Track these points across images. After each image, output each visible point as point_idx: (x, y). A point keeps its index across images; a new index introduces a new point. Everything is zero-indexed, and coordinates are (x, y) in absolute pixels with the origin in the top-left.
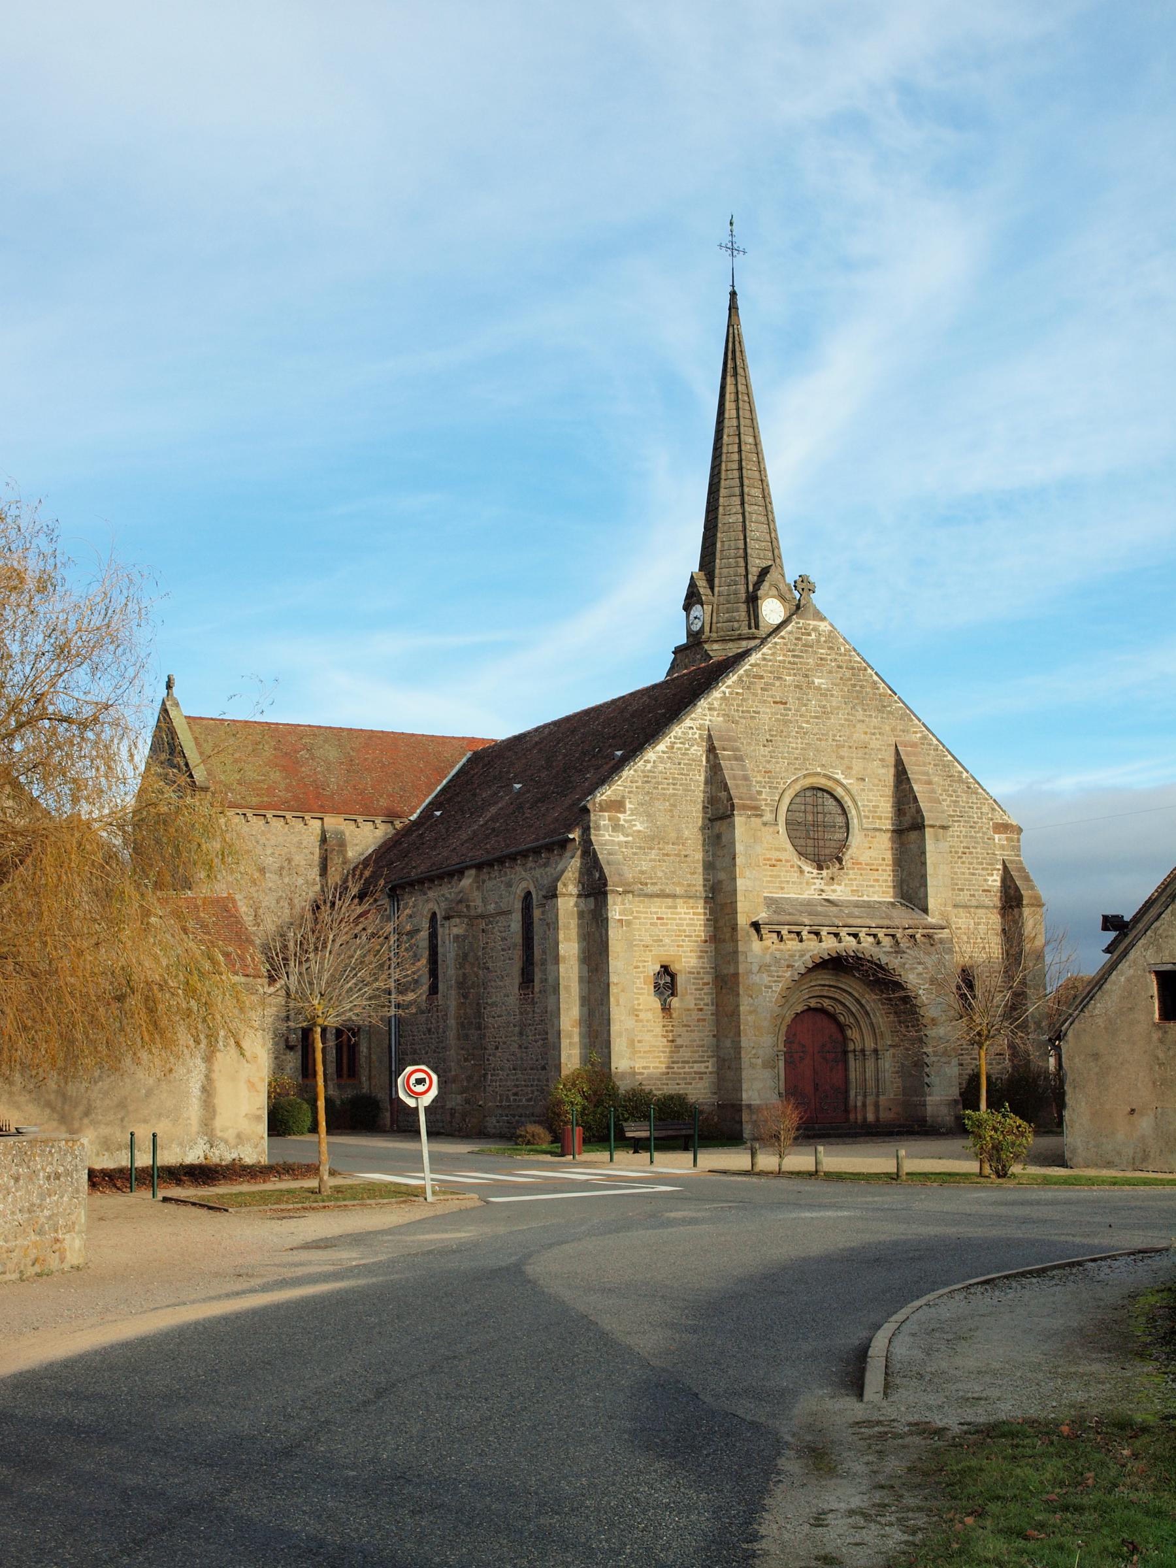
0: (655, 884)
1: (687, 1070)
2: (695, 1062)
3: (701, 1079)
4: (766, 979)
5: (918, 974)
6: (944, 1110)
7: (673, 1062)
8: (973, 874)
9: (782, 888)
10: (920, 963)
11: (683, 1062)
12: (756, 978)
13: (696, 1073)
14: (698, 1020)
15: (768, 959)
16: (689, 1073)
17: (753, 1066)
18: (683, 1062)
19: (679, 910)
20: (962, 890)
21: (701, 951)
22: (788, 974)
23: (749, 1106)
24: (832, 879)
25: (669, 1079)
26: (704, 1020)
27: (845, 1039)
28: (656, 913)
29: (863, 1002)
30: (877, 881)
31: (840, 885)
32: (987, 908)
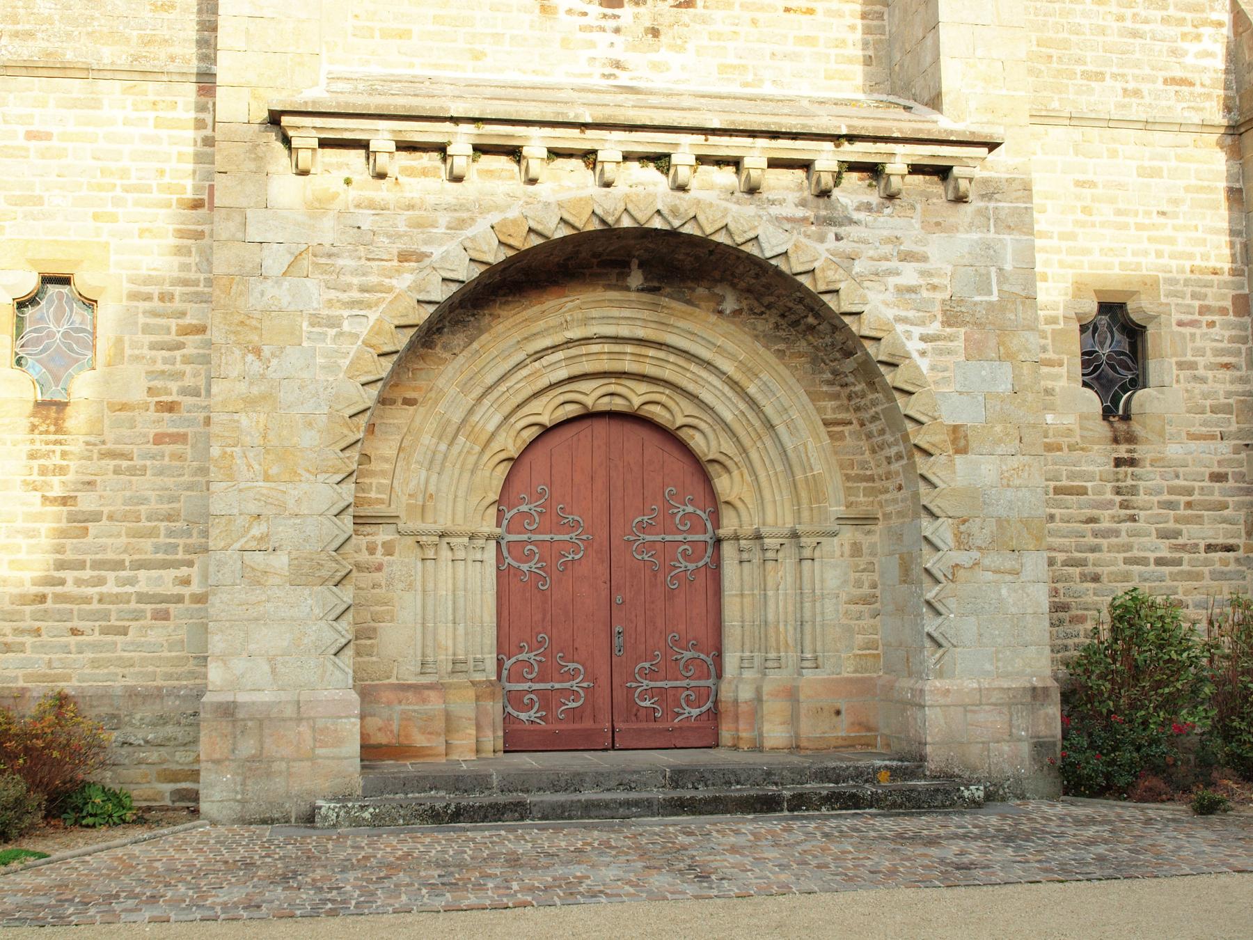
0: (30, 34)
1: (111, 588)
3: (164, 616)
4: (314, 293)
5: (900, 290)
6: (990, 721)
7: (61, 565)
8: (1135, 34)
10: (907, 257)
11: (97, 565)
12: (278, 294)
13: (142, 598)
14: (159, 439)
15: (328, 232)
16: (117, 599)
17: (256, 579)
18: (97, 565)
20: (1100, 76)
21: (182, 234)
22: (404, 281)
23: (228, 711)
24: (655, 32)
25: (45, 616)
26: (180, 438)
27: (714, 504)
29: (752, 390)
30: (810, 40)
31: (681, 49)
32: (1181, 127)
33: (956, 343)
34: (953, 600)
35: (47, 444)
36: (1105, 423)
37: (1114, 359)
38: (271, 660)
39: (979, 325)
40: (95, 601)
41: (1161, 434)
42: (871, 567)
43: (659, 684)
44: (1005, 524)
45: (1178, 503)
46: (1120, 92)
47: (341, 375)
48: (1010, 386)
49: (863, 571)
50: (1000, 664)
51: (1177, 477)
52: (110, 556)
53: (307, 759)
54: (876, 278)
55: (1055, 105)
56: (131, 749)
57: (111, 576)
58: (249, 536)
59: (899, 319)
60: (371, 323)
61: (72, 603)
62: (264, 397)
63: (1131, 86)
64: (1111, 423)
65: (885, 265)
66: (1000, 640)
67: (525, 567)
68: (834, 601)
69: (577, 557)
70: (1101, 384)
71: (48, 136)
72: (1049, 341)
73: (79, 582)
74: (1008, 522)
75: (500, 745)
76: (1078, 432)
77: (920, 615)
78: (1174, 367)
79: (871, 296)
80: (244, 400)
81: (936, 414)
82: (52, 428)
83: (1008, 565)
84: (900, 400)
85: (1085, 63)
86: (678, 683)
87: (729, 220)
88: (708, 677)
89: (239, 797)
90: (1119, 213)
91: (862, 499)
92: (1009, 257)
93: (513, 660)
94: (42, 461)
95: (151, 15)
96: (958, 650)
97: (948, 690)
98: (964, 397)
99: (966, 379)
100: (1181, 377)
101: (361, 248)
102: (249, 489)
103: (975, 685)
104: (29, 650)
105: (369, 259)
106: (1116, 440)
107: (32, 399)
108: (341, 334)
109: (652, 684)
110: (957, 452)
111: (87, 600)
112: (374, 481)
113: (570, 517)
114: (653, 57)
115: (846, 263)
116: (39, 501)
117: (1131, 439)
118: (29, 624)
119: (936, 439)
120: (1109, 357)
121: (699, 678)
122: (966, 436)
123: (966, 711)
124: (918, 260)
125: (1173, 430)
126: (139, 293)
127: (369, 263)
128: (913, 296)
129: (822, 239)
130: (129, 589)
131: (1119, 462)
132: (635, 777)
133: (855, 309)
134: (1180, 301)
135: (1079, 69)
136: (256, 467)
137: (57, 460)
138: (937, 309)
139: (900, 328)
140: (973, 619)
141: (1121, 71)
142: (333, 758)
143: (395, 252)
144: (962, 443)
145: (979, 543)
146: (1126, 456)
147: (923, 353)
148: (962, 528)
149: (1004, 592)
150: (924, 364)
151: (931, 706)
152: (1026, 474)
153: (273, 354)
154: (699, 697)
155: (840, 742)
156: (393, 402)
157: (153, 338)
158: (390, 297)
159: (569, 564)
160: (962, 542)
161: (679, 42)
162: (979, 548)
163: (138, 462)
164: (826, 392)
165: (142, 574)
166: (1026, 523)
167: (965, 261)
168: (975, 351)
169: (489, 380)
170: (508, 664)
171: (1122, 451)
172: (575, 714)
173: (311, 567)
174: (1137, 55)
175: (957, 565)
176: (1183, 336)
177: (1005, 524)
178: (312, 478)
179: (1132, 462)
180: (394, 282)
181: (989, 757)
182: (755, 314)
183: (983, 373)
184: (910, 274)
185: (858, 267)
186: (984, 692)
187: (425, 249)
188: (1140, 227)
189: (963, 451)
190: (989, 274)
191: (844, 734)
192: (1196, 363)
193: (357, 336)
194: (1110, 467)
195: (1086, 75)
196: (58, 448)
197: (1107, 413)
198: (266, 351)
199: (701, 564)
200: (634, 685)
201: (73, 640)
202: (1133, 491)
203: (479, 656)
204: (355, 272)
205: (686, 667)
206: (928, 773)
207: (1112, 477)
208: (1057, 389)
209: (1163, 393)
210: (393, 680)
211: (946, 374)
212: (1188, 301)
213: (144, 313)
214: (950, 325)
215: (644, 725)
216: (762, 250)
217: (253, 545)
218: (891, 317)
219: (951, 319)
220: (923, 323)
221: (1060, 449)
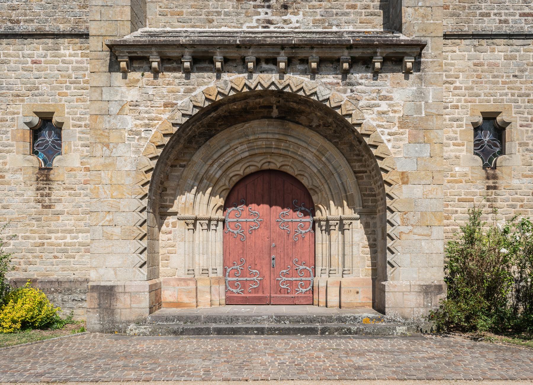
0: (32, 21)
1: (68, 240)
2: (80, 232)
9: (211, 21)
10: (385, 98)
11: (64, 231)
13: (80, 244)
16: (70, 245)
18: (64, 231)
19: (62, 51)
20: (488, 15)
22: (165, 116)
28: (30, 56)
31: (295, 14)
33: (404, 136)
34: (400, 247)
35: (43, 184)
36: (483, 171)
37: (490, 142)
38: (115, 269)
39: (416, 128)
40: (63, 245)
41: (509, 175)
42: (373, 232)
43: (289, 279)
44: (424, 214)
45: (516, 205)
46: (498, 21)
47: (141, 155)
48: (429, 154)
49: (370, 234)
50: (420, 275)
51: (516, 194)
52: (68, 228)
53: (128, 308)
54: (369, 108)
55: (466, 29)
56: (76, 302)
57: (68, 235)
58: (105, 220)
59: (379, 126)
60: (153, 133)
61: (54, 246)
62: (110, 164)
63: (503, 18)
64: (486, 171)
65: (373, 102)
66: (420, 264)
67: (235, 232)
68: (357, 246)
69: (256, 228)
70: (484, 154)
71: (40, 62)
72: (458, 135)
73: (56, 238)
74: (426, 214)
75: (223, 302)
76: (470, 174)
77: (386, 254)
78: (517, 145)
79: (366, 116)
80: (102, 165)
81: (394, 167)
82: (45, 178)
83: (425, 232)
84: (379, 162)
85: (481, 9)
86: (297, 279)
87: (303, 85)
88: (310, 276)
89: (102, 323)
90: (495, 77)
91: (370, 204)
92: (431, 97)
93: (231, 269)
94: (41, 191)
95: (78, 10)
96: (401, 268)
97: (396, 285)
98: (408, 160)
99: (408, 151)
100: (521, 149)
101: (148, 102)
102: (105, 201)
103: (408, 284)
104: (38, 264)
105: (152, 107)
106: (488, 178)
107: (38, 166)
108: (141, 138)
109: (286, 279)
110: (403, 183)
111: (59, 245)
112: (168, 198)
113: (254, 212)
114: (285, 18)
115: (354, 102)
116: (40, 207)
117: (495, 177)
118: (38, 254)
119: (394, 178)
120: (488, 142)
121: (306, 277)
122: (407, 177)
123: (403, 294)
124: (389, 100)
125: (515, 173)
126: (77, 124)
127: (152, 108)
128: (385, 116)
129: (345, 92)
130: (75, 241)
131: (488, 188)
132: (260, 318)
133: (359, 122)
134: (522, 115)
135: (478, 12)
136: (108, 192)
137: (47, 191)
138: (396, 121)
139: (379, 130)
140: (408, 255)
141: (499, 11)
142: (138, 308)
143: (162, 103)
144: (406, 179)
145: (412, 223)
146: (492, 185)
147: (389, 141)
148: (405, 216)
149: (423, 244)
150: (389, 146)
151: (388, 292)
152: (435, 193)
153: (114, 147)
154: (306, 285)
155: (358, 305)
156: (176, 166)
157: (83, 142)
158: (160, 122)
159: (253, 231)
160: (405, 223)
161: (296, 10)
162: (412, 225)
163: (78, 191)
164: (356, 159)
165: (80, 235)
166: (434, 213)
167: (410, 99)
168: (414, 140)
169: (215, 157)
170: (229, 270)
171: (491, 183)
172: (256, 290)
173: (130, 232)
174: (507, 4)
175: (402, 232)
176: (522, 131)
177: (424, 214)
178: (130, 197)
179: (495, 188)
180: (162, 116)
181: (413, 314)
182: (326, 127)
183: (417, 149)
184: (384, 106)
185: (361, 103)
186: (412, 287)
187: (175, 102)
188: (504, 83)
189: (405, 183)
190: (421, 105)
191: (360, 301)
192: (528, 143)
193: (147, 138)
194: (485, 190)
195: (482, 15)
196: (47, 186)
197: (485, 167)
198: (111, 146)
199: (307, 231)
200: (280, 279)
201: (55, 260)
202: (495, 200)
203: (214, 267)
204: (146, 112)
205: (301, 272)
206: (386, 320)
207: (485, 194)
208: (461, 156)
209: (511, 157)
210: (176, 277)
211: (399, 149)
212: (526, 115)
213: (79, 132)
214: (402, 128)
215: (283, 295)
216: (318, 98)
217: (107, 223)
218: (375, 125)
219: (403, 124)
220: (390, 128)
221: (461, 182)
